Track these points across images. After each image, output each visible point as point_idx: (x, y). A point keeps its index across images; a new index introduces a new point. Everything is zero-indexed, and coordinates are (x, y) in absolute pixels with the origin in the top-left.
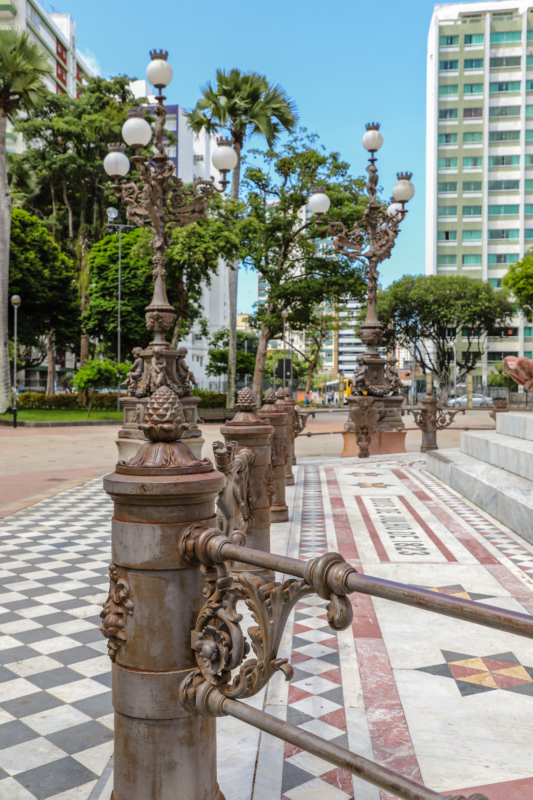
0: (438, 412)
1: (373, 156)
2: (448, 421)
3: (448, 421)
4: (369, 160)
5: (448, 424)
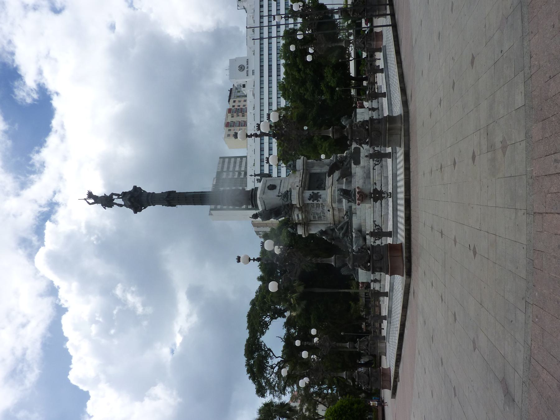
0: (375, 231)
1: (252, 260)
2: (378, 227)
3: (378, 227)
4: (254, 261)
5: (380, 227)
